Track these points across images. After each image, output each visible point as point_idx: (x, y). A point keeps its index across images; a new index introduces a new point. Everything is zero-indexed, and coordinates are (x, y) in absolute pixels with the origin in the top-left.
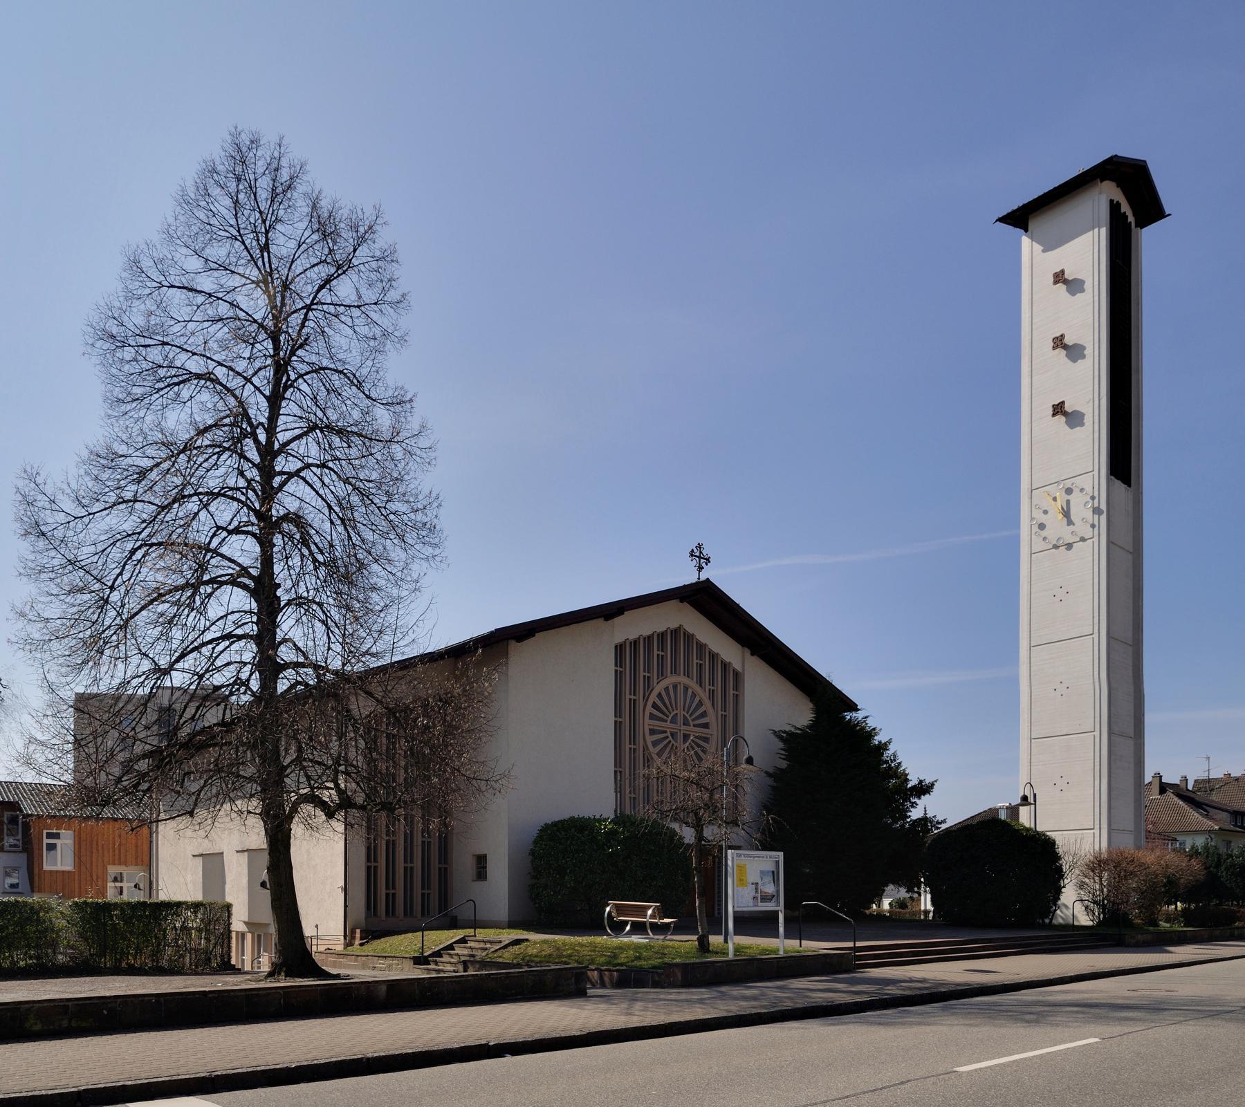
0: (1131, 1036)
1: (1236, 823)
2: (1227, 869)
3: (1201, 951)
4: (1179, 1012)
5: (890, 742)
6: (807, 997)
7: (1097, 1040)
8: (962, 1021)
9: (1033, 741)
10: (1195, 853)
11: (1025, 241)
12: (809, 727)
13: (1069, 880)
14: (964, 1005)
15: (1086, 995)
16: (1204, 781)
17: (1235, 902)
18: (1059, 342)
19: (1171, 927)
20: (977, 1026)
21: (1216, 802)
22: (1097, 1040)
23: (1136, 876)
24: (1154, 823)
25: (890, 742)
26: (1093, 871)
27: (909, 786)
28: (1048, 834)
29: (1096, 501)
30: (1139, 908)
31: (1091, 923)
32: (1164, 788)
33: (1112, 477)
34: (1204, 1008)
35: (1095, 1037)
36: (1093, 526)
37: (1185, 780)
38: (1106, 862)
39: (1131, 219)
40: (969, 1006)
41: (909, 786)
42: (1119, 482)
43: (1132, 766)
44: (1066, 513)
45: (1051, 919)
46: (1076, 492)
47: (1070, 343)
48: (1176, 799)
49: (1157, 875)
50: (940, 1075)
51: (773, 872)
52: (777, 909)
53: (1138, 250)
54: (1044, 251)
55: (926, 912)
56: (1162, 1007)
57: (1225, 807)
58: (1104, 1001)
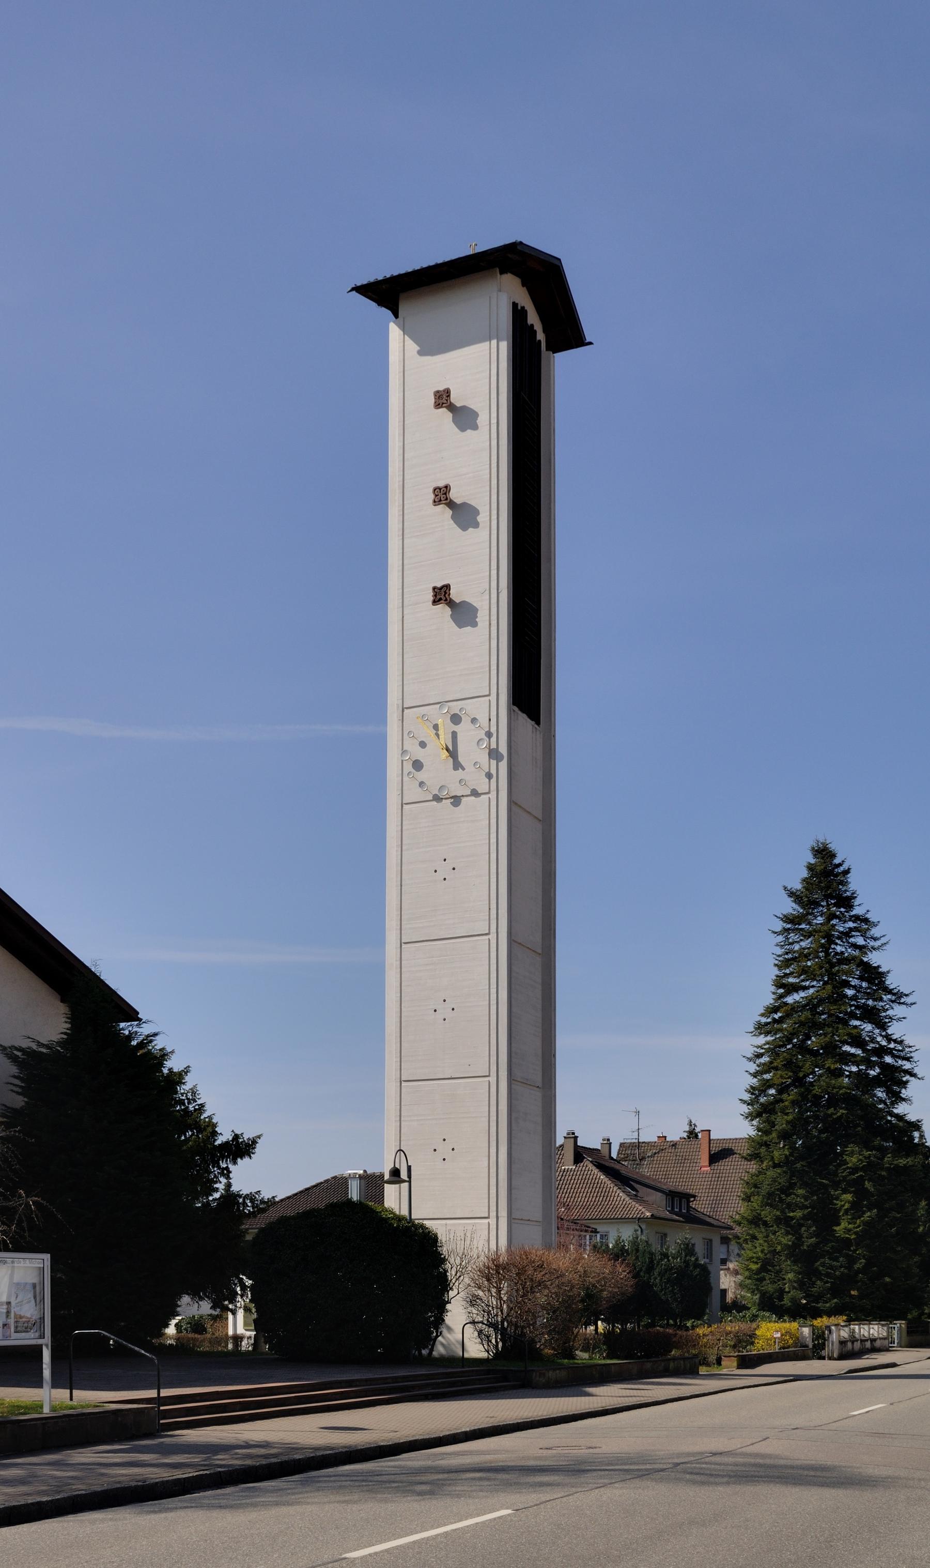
0: (549, 1505)
1: (673, 1208)
2: (661, 1274)
3: (628, 1392)
4: (603, 1473)
5: (186, 1071)
6: (103, 1475)
7: (509, 1511)
8: (332, 1498)
9: (404, 1084)
10: (619, 1254)
11: (394, 331)
12: (61, 1043)
13: (455, 1292)
14: (330, 1476)
15: (488, 1457)
16: (632, 1146)
17: (671, 1322)
18: (442, 495)
19: (591, 1358)
20: (355, 1502)
21: (648, 1178)
22: (509, 1511)
23: (546, 1287)
24: (568, 1207)
25: (186, 1071)
26: (488, 1280)
27: (218, 1143)
28: (427, 1223)
29: (494, 739)
30: (549, 1333)
31: (485, 1355)
32: (580, 1154)
33: (516, 708)
34: (632, 1467)
35: (507, 1508)
36: (489, 776)
37: (608, 1143)
38: (505, 1267)
39: (541, 336)
40: (337, 1478)
41: (216, 1143)
42: (525, 716)
43: (540, 1128)
44: (453, 753)
45: (432, 1350)
46: (466, 723)
47: (458, 501)
48: (596, 1171)
49: (573, 1287)
50: (329, 1563)
51: (34, 1286)
52: (40, 1342)
53: (549, 381)
54: (420, 353)
55: (237, 1339)
56: (583, 1467)
57: (659, 1185)
58: (513, 1464)
